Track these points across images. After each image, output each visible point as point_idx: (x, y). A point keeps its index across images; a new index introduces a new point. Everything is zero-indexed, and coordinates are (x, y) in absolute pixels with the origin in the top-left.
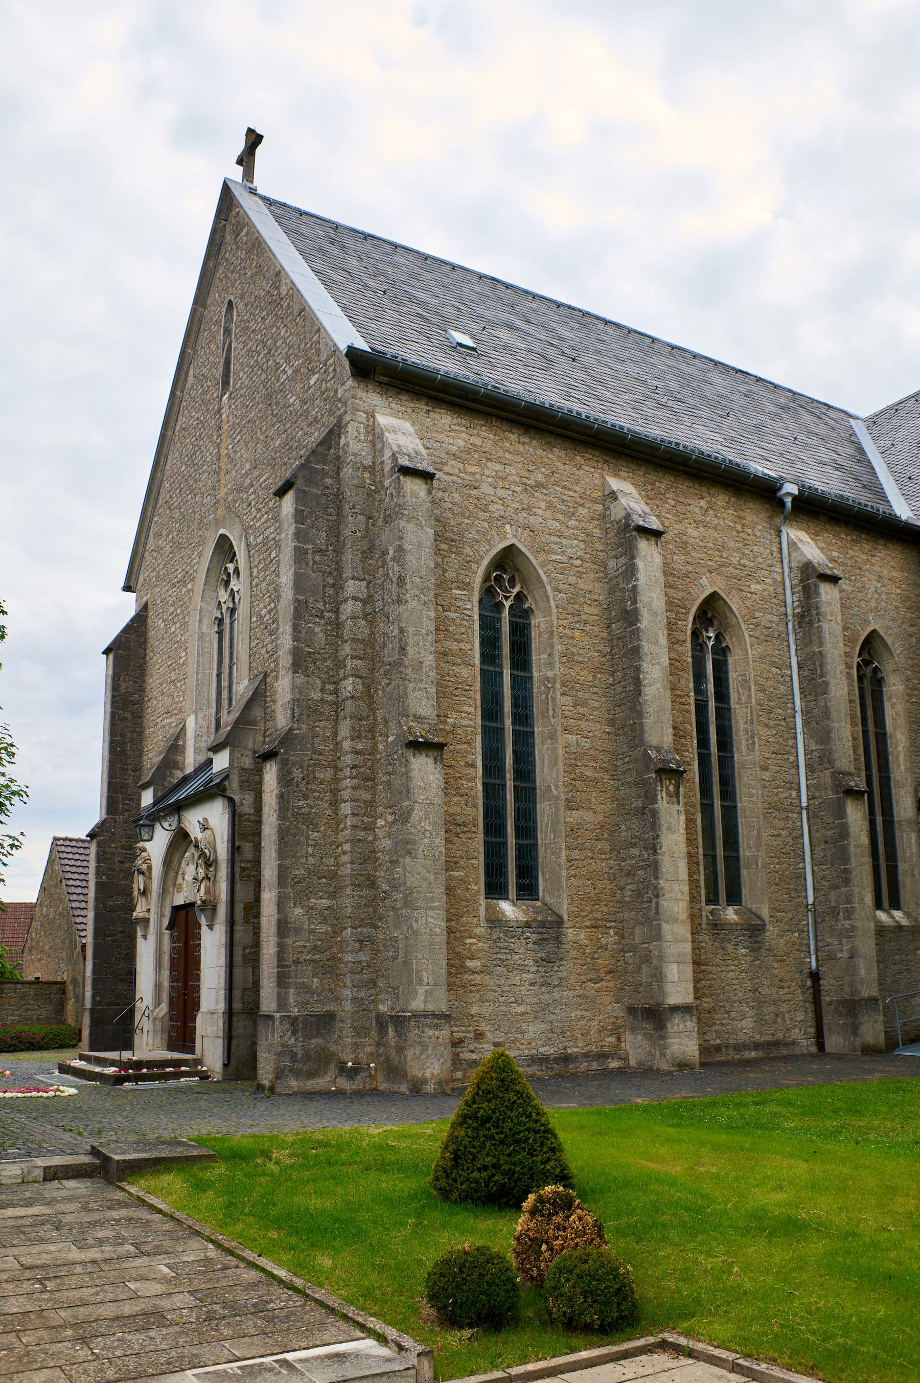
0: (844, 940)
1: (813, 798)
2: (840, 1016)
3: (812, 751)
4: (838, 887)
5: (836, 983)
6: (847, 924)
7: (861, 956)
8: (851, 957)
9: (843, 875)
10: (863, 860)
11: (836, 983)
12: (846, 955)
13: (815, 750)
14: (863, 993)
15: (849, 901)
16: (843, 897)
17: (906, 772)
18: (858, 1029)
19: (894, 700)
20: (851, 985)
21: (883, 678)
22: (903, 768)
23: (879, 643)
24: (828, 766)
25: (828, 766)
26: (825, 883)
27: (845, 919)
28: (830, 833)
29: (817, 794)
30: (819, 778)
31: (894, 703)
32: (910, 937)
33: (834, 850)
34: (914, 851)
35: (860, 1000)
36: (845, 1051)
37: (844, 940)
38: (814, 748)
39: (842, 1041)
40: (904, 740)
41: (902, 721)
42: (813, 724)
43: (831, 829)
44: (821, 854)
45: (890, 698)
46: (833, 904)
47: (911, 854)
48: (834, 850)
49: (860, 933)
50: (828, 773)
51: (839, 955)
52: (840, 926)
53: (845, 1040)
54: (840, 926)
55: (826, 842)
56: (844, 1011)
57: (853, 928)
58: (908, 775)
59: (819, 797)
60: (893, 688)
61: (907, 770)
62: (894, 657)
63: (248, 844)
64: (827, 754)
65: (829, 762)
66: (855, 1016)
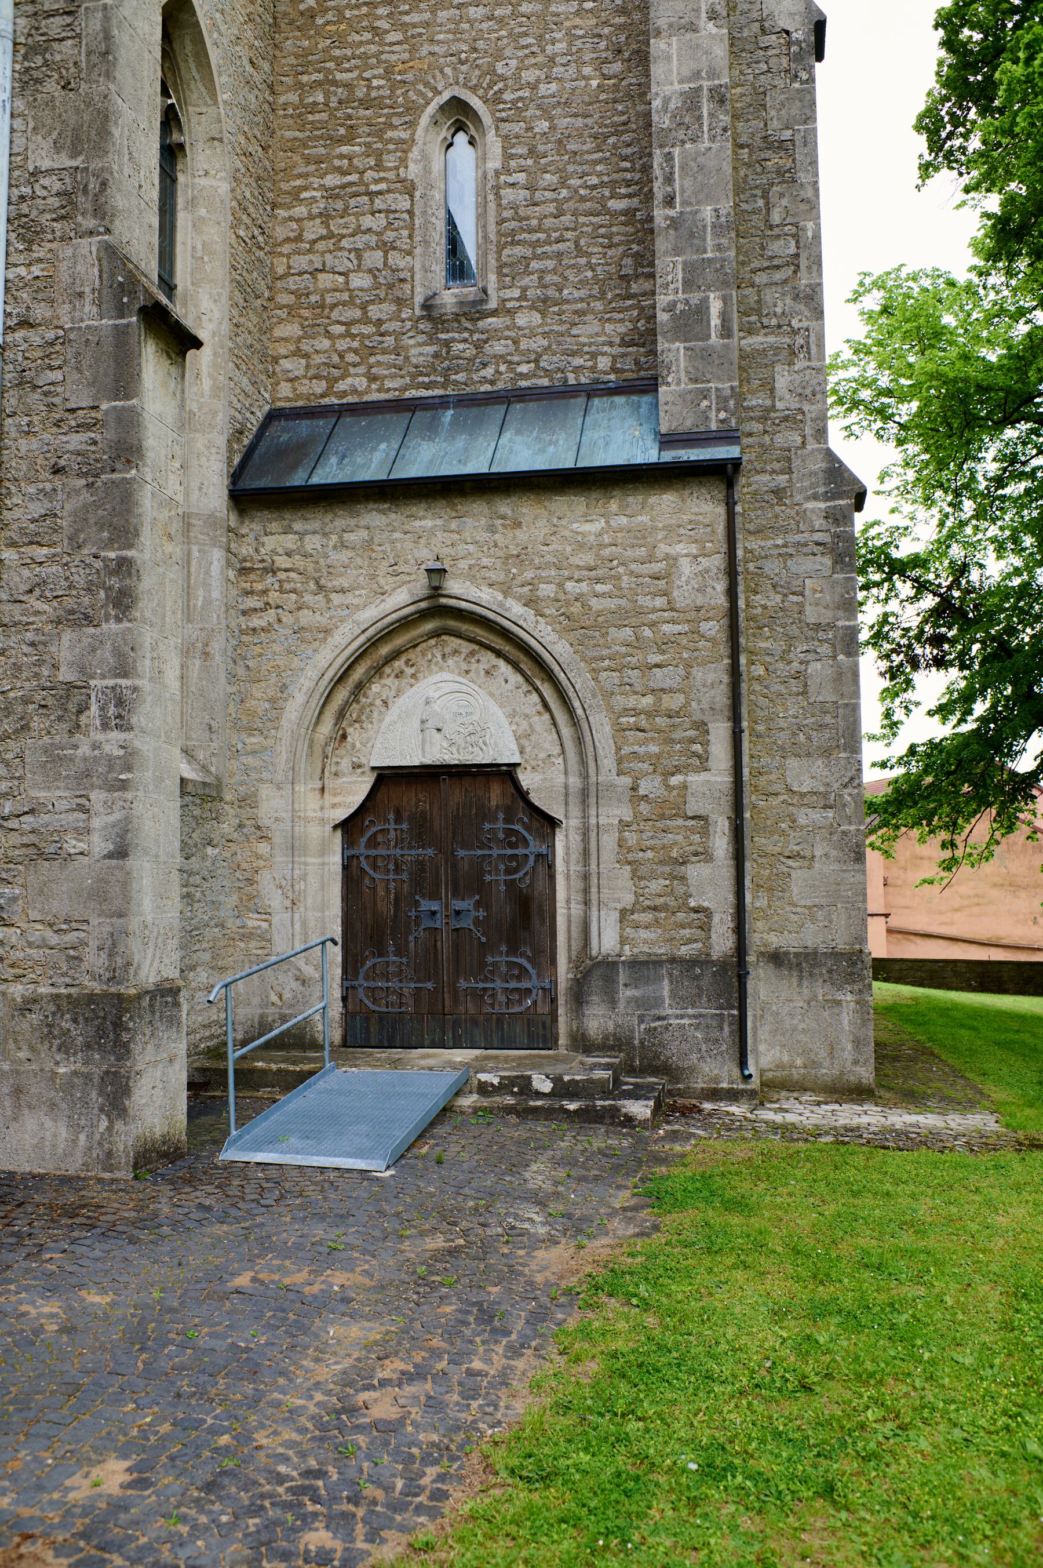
0: (98, 796)
1: (25, 323)
2: (64, 1048)
3: (36, 174)
4: (88, 620)
5: (54, 939)
6: (112, 742)
7: (146, 852)
8: (121, 853)
9: (114, 582)
10: (169, 548)
11: (54, 939)
12: (99, 845)
13: (50, 172)
14: (142, 974)
15: (123, 670)
16: (106, 653)
17: (215, 396)
18: (126, 1091)
19: (203, 212)
20: (112, 946)
21: (181, 147)
22: (207, 384)
23: (189, 48)
24: (90, 223)
25: (90, 223)
26: (40, 606)
27: (105, 726)
28: (76, 441)
29: (40, 312)
30: (53, 261)
31: (201, 219)
32: (197, 812)
33: (86, 497)
34: (215, 594)
35: (139, 997)
36: (73, 1167)
37: (98, 796)
38: (46, 164)
39: (63, 1133)
40: (217, 315)
41: (218, 269)
42: (51, 86)
43: (80, 427)
44: (37, 509)
45: (192, 203)
46: (66, 675)
47: (208, 602)
48: (86, 497)
49: (149, 774)
50: (89, 247)
51: (73, 845)
52: (84, 750)
53: (75, 1128)
54: (84, 750)
55: (57, 471)
56: (78, 1033)
57: (129, 760)
58: (220, 405)
59: (46, 323)
60: (203, 181)
61: (216, 390)
62: (216, 102)
63: (649, 1112)
64: (93, 185)
65: (99, 211)
66: (122, 1050)
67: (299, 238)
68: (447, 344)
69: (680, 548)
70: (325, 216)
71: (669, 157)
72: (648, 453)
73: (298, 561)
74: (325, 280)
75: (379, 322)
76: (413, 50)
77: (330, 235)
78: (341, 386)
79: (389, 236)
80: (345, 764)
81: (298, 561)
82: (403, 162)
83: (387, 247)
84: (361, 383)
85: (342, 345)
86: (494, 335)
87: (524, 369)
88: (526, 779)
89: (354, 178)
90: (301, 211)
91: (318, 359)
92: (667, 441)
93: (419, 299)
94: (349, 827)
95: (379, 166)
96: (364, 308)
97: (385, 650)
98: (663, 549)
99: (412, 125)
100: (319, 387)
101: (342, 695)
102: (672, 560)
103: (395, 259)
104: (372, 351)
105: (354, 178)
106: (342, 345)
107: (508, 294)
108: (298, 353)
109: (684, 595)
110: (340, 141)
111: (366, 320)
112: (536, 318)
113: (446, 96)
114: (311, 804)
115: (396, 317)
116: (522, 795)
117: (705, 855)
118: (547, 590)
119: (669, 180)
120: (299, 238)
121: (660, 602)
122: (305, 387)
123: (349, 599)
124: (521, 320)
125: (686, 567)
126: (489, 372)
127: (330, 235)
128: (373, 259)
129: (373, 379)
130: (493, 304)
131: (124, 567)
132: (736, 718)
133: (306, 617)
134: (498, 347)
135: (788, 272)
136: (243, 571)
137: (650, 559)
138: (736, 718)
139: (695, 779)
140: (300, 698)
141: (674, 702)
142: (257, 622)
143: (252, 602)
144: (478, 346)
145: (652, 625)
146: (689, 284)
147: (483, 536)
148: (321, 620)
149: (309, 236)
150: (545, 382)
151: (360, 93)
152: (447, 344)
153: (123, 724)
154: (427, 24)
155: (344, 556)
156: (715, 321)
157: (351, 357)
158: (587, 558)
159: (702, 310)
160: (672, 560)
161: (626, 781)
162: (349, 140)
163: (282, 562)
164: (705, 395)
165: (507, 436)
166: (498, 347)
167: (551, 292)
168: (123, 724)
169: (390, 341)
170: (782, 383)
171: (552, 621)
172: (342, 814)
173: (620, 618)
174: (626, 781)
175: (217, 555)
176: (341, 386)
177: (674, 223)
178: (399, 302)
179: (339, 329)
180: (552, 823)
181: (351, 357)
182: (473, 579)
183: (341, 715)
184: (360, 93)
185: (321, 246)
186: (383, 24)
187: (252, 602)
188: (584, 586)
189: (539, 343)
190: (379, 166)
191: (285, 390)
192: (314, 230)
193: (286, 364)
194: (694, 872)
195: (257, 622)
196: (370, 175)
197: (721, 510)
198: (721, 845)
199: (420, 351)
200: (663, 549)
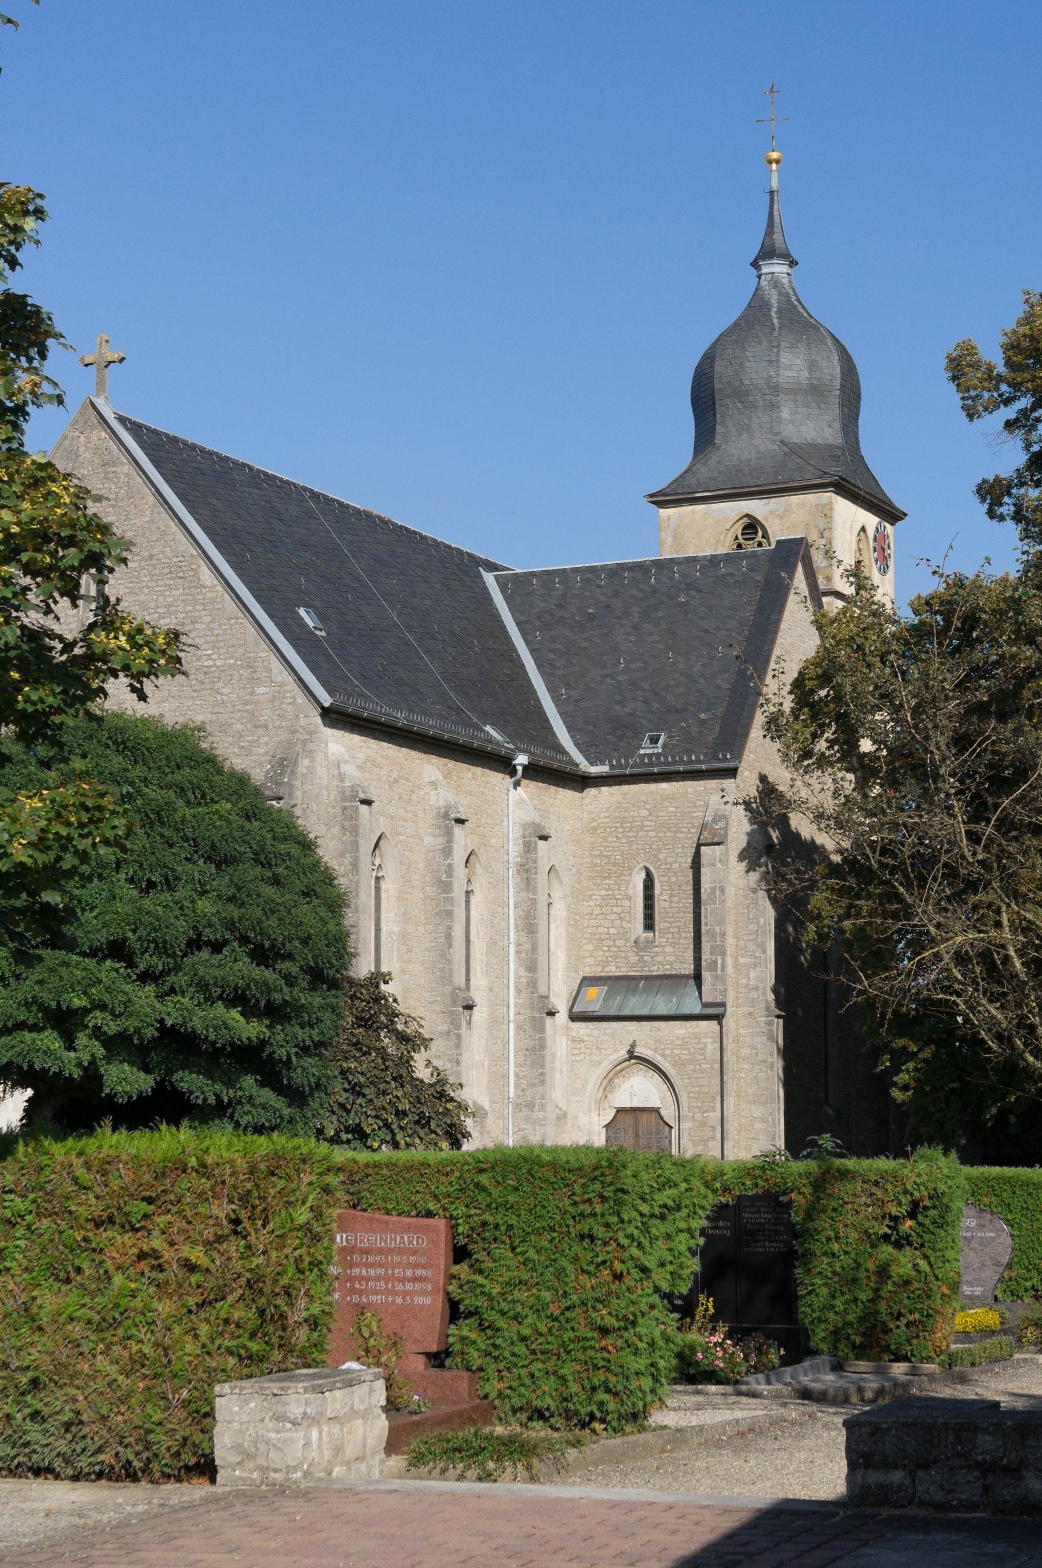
0: (538, 1127)
6: (541, 1115)
22: (560, 981)
67: (591, 914)
68: (642, 956)
69: (708, 1040)
70: (601, 906)
71: (706, 909)
72: (697, 1009)
73: (591, 1038)
74: (601, 930)
75: (619, 947)
76: (630, 846)
77: (602, 914)
78: (607, 969)
79: (623, 915)
80: (607, 1106)
81: (591, 1038)
82: (627, 888)
83: (621, 919)
84: (614, 969)
85: (607, 954)
86: (657, 954)
87: (667, 967)
88: (663, 1113)
89: (610, 892)
90: (592, 903)
91: (599, 958)
92: (706, 1005)
93: (633, 940)
94: (607, 1126)
95: (619, 889)
96: (614, 941)
97: (619, 1068)
98: (703, 1040)
99: (631, 875)
100: (599, 969)
101: (605, 1082)
102: (706, 1044)
103: (625, 924)
104: (617, 957)
105: (610, 892)
106: (607, 954)
107: (662, 940)
108: (592, 956)
109: (708, 1056)
110: (605, 878)
111: (615, 945)
112: (672, 949)
113: (642, 865)
114: (595, 1119)
115: (625, 945)
116: (662, 1118)
117: (713, 1138)
118: (668, 1052)
119: (706, 917)
120: (591, 914)
121: (702, 1057)
122: (594, 968)
123: (608, 1052)
124: (667, 949)
125: (709, 1047)
126: (656, 968)
127: (602, 914)
128: (618, 923)
129: (617, 967)
130: (657, 943)
131: (542, 1074)
132: (722, 1096)
133: (594, 1057)
134: (659, 959)
135: (754, 936)
136: (573, 1041)
137: (699, 1043)
138: (722, 1096)
139: (711, 1114)
140: (592, 1084)
141: (706, 1089)
142: (578, 1058)
143: (576, 1052)
144: (652, 958)
145: (700, 1065)
146: (712, 953)
147: (648, 1033)
148: (598, 1058)
149: (595, 913)
150: (674, 972)
151: (612, 860)
152: (642, 956)
153: (543, 1110)
154: (634, 837)
155: (606, 1037)
156: (719, 966)
157: (610, 959)
158: (680, 1042)
159: (716, 962)
160: (706, 1044)
161: (691, 1114)
162: (609, 878)
163: (586, 1038)
164: (716, 990)
165: (659, 996)
166: (659, 959)
167: (676, 941)
168: (543, 1110)
169: (623, 954)
170: (752, 975)
171: (669, 1062)
172: (606, 1123)
173: (690, 1062)
174: (691, 1114)
175: (565, 1038)
176: (607, 969)
177: (708, 932)
178: (626, 940)
179: (605, 948)
180: (671, 1127)
181: (610, 959)
182: (645, 1047)
183: (605, 1089)
184: (612, 860)
185: (599, 917)
186: (620, 835)
187: (576, 1052)
188: (679, 1052)
189: (672, 959)
190: (619, 889)
191: (587, 969)
192: (597, 911)
193: (588, 960)
194: (711, 1144)
195: (578, 1058)
196: (616, 892)
197: (718, 1027)
198: (719, 1135)
199: (634, 959)
200: (703, 1040)
